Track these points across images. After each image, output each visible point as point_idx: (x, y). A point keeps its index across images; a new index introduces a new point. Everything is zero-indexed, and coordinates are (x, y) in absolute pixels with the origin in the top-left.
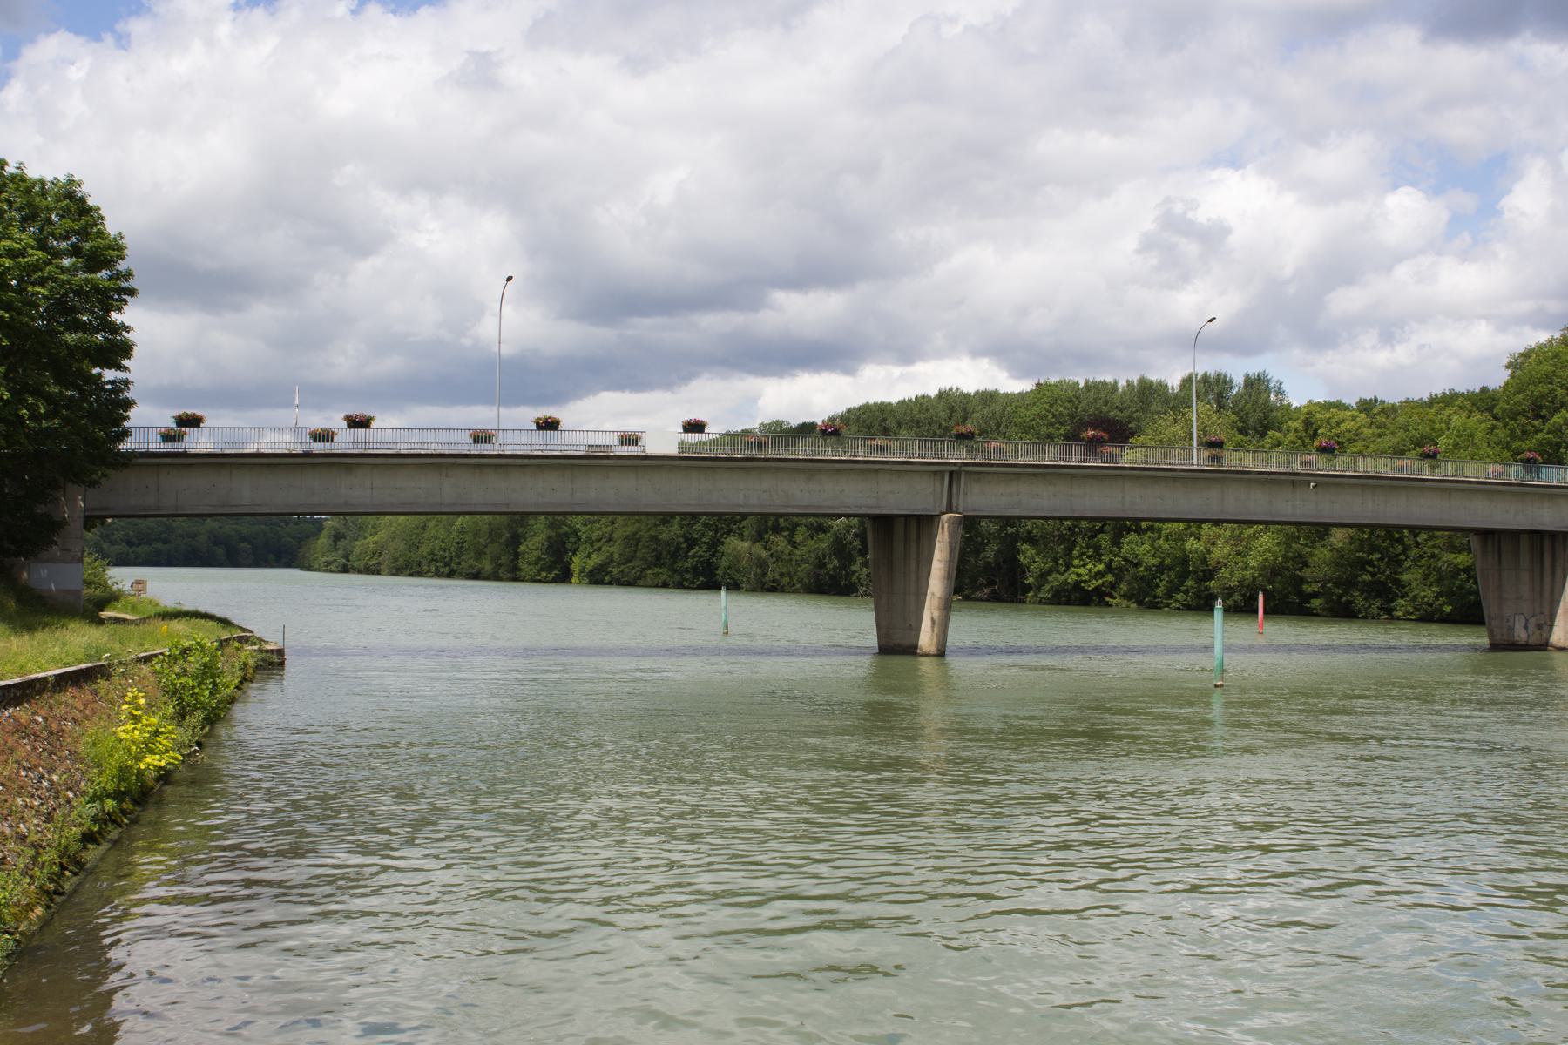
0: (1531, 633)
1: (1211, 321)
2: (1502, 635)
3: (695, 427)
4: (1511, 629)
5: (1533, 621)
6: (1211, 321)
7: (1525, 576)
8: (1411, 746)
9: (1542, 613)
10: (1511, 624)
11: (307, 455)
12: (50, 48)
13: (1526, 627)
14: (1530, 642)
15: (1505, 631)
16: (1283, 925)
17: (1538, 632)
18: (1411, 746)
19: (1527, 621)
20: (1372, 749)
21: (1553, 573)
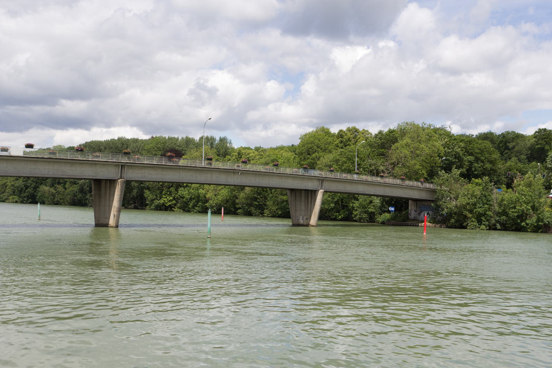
1: (209, 119)
2: (296, 221)
4: (298, 220)
5: (305, 217)
6: (209, 119)
7: (303, 204)
10: (298, 218)
13: (303, 219)
14: (304, 224)
15: (297, 220)
17: (306, 221)
19: (303, 217)
21: (311, 203)
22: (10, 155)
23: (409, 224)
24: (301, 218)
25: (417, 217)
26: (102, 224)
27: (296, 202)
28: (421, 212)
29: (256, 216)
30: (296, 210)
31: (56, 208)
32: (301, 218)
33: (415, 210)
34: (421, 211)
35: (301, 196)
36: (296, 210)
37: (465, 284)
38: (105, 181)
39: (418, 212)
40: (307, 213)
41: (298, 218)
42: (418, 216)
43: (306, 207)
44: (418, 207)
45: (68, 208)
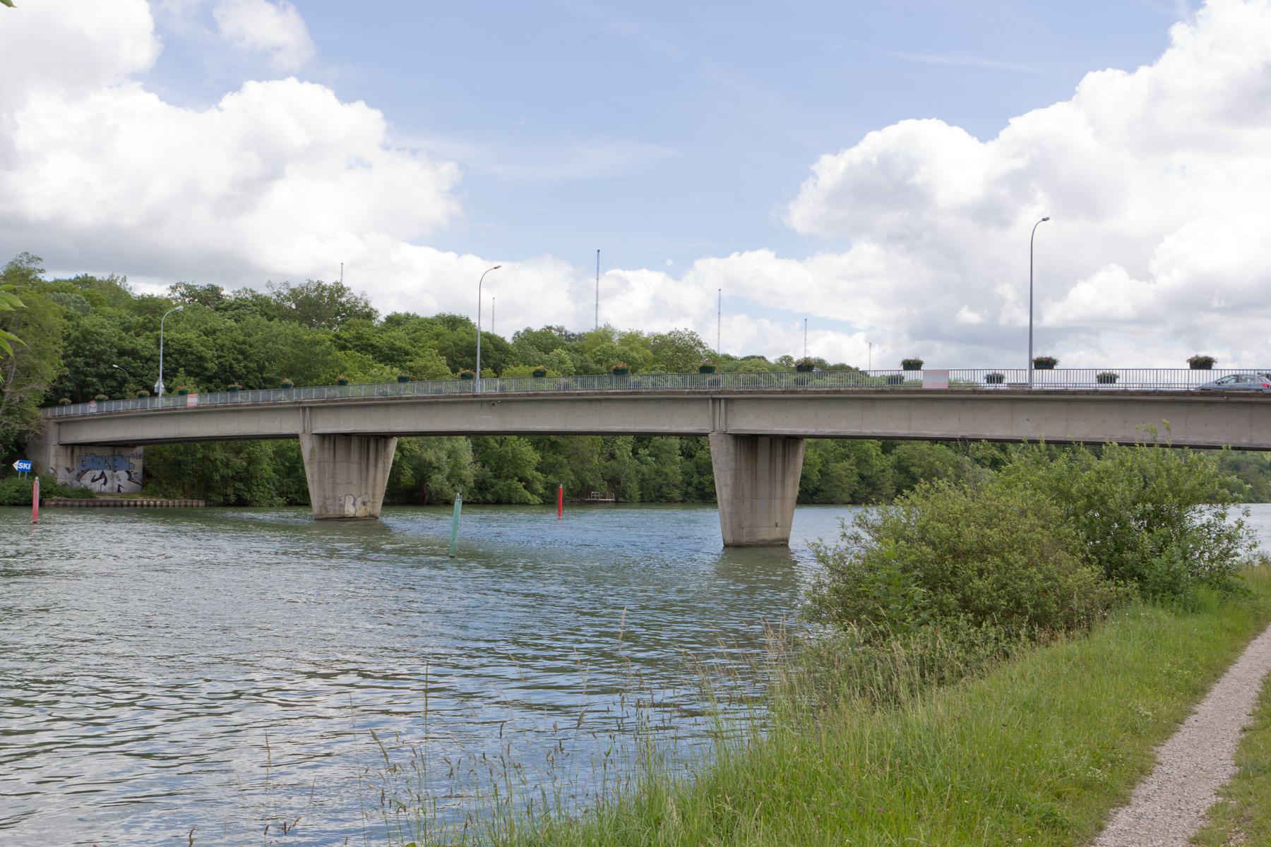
0: (357, 508)
1: (1044, 220)
2: (335, 511)
3: (1202, 364)
4: (342, 506)
5: (359, 500)
6: (1044, 220)
7: (354, 467)
8: (530, 707)
9: (366, 494)
10: (342, 502)
11: (1096, 392)
12: (644, 270)
13: (354, 504)
14: (357, 515)
15: (337, 508)
16: (483, 723)
17: (363, 507)
18: (530, 707)
19: (355, 499)
20: (402, 654)
21: (376, 466)
22: (1202, 378)
23: (125, 503)
24: (349, 501)
25: (71, 483)
26: (763, 540)
27: (334, 462)
28: (84, 472)
29: (97, 509)
30: (334, 483)
31: (827, 510)
32: (349, 501)
33: (69, 466)
34: (83, 469)
35: (349, 450)
36: (334, 483)
37: (748, 673)
38: (768, 439)
39: (76, 473)
40: (366, 489)
41: (342, 502)
42: (75, 482)
43: (364, 476)
44: (75, 460)
45: (97, 518)
